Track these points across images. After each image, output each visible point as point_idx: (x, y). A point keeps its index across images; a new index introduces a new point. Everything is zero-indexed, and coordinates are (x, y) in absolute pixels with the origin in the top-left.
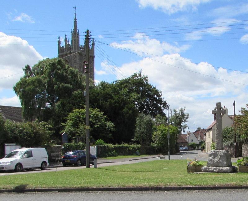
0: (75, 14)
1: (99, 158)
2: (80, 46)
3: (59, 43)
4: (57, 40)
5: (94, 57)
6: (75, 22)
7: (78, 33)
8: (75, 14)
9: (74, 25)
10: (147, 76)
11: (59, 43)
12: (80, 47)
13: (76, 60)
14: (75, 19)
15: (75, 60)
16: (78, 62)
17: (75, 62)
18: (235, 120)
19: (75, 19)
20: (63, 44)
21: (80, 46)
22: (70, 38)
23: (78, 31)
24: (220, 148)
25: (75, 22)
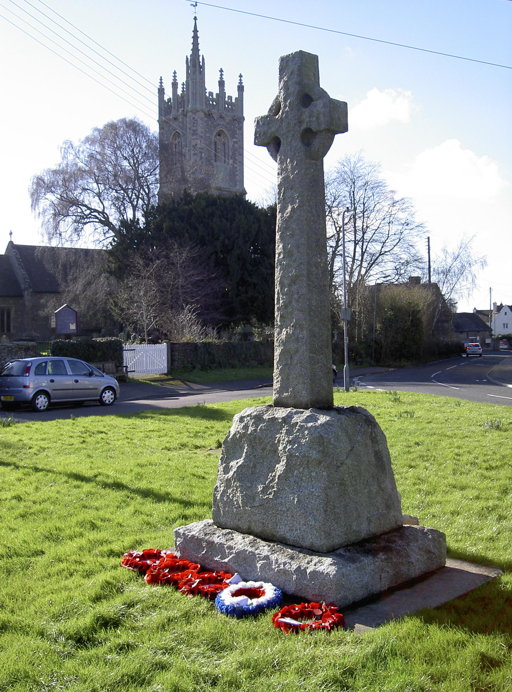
0: (195, 19)
1: (23, 414)
2: (207, 95)
3: (161, 91)
4: (158, 85)
5: (243, 119)
6: (195, 38)
7: (201, 64)
8: (195, 19)
9: (191, 46)
10: (94, 198)
11: (161, 91)
12: (226, 103)
13: (196, 130)
14: (195, 31)
15: (195, 128)
16: (202, 135)
17: (195, 133)
18: (311, 376)
19: (195, 31)
20: (168, 94)
21: (226, 99)
22: (182, 78)
23: (201, 60)
24: (305, 396)
25: (195, 38)
